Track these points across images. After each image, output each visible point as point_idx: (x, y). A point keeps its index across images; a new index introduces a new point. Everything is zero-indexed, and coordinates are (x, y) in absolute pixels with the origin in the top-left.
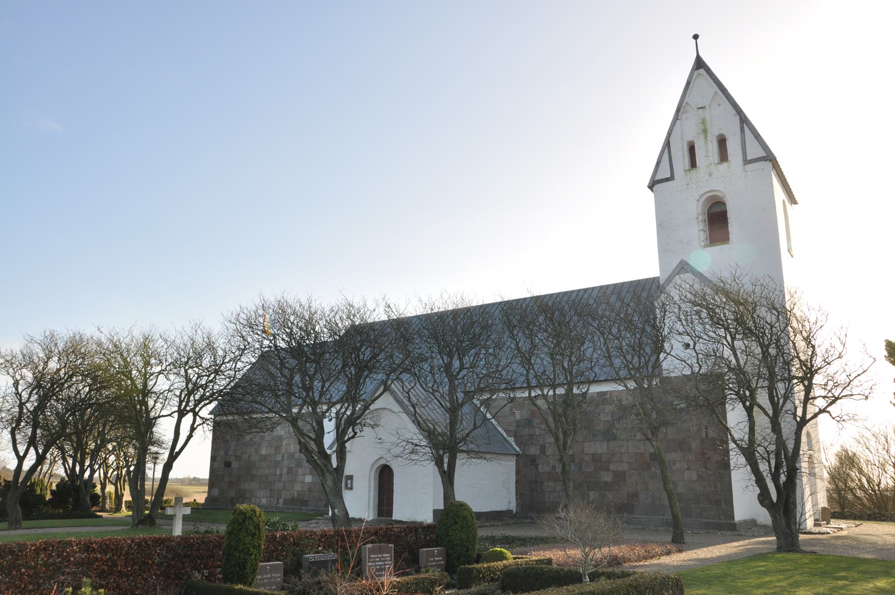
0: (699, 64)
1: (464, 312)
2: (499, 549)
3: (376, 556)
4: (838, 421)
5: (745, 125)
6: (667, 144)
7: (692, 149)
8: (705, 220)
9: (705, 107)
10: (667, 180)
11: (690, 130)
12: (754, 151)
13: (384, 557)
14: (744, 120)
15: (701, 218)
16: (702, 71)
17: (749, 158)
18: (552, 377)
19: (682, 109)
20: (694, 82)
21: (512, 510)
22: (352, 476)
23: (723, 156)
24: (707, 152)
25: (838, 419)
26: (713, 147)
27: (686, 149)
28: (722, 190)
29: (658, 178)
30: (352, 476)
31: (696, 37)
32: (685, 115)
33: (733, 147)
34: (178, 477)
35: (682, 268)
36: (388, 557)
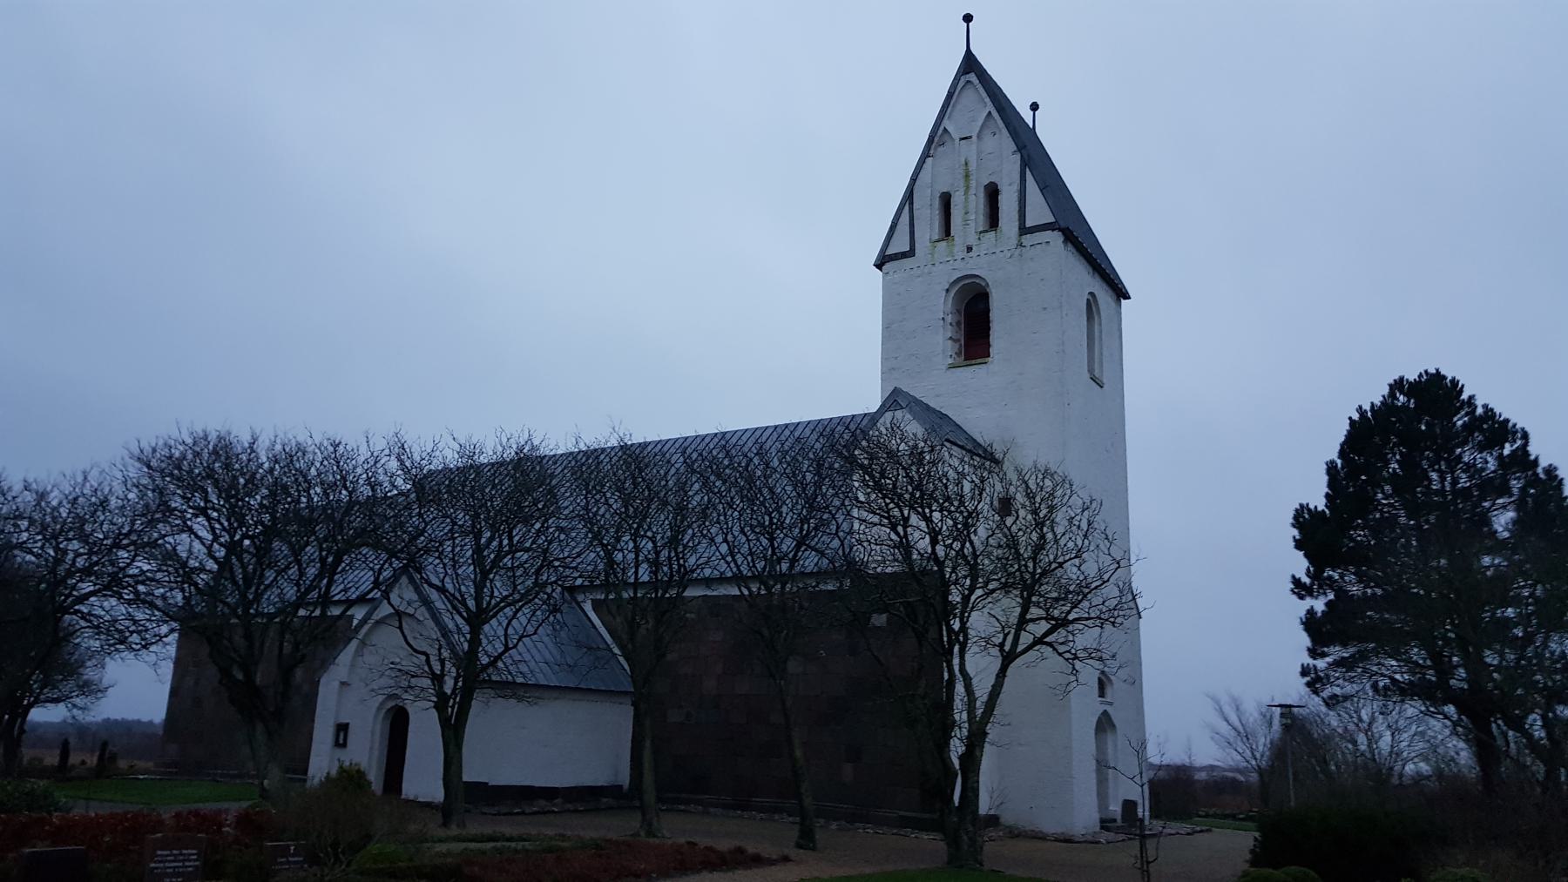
0: (970, 64)
1: (595, 454)
2: (1464, 871)
3: (168, 852)
4: (1067, 660)
5: (1027, 169)
6: (909, 197)
7: (946, 200)
8: (958, 323)
9: (971, 137)
10: (904, 255)
11: (942, 176)
13: (184, 855)
15: (949, 319)
16: (972, 77)
17: (1029, 224)
18: (387, 566)
19: (936, 139)
20: (959, 93)
21: (621, 786)
22: (347, 724)
24: (968, 211)
25: (1067, 655)
26: (978, 202)
27: (937, 203)
29: (889, 252)
30: (347, 724)
31: (968, 18)
32: (941, 149)
35: (895, 400)
36: (193, 854)
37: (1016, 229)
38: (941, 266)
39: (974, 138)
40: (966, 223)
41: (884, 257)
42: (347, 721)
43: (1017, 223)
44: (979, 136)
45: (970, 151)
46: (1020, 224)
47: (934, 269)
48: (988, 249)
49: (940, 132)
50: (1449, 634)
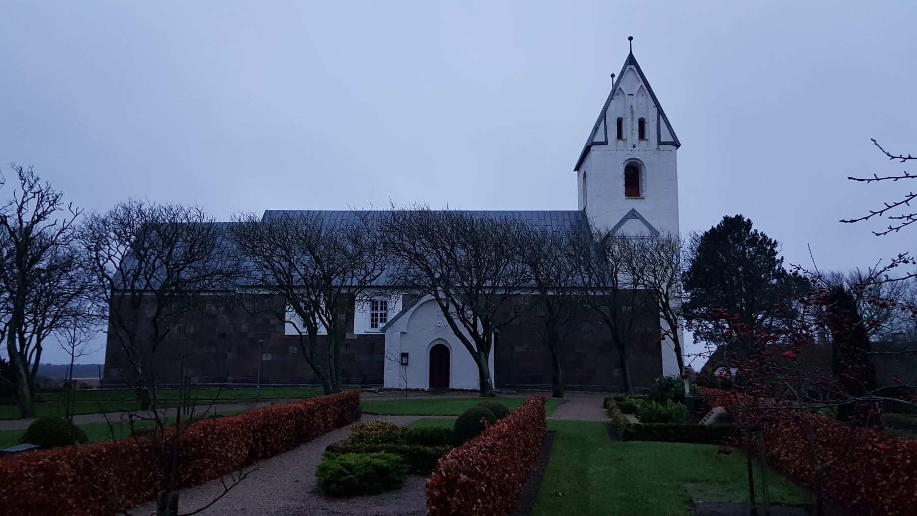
0: (631, 60)
6: (603, 116)
7: (620, 122)
9: (633, 95)
10: (602, 143)
12: (666, 137)
14: (660, 112)
17: (662, 140)
22: (408, 354)
23: (642, 136)
24: (632, 130)
28: (453, 350)
29: (595, 140)
30: (408, 354)
31: (631, 39)
33: (651, 129)
34: (64, 364)
37: (656, 142)
38: (620, 152)
39: (635, 95)
40: (632, 134)
41: (592, 142)
42: (408, 352)
43: (657, 139)
44: (637, 95)
45: (633, 101)
46: (658, 140)
47: (617, 152)
48: (643, 148)
49: (618, 88)
50: (846, 325)
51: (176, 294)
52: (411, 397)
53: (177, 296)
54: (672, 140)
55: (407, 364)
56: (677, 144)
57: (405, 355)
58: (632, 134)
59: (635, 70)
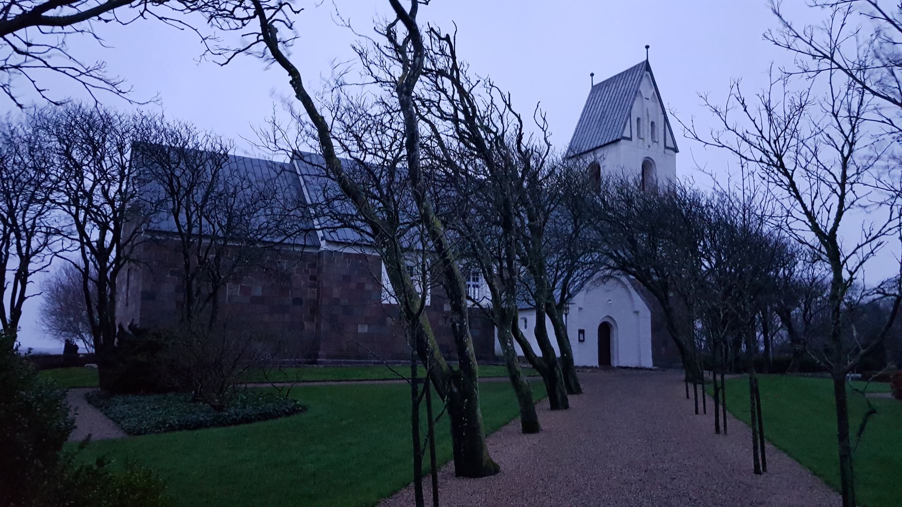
7: (638, 119)
12: (670, 144)
31: (647, 47)
40: (648, 136)
51: (758, 279)
52: (641, 372)
53: (652, 267)
54: (673, 147)
55: (584, 340)
56: (676, 150)
57: (581, 332)
58: (648, 136)
59: (650, 77)
